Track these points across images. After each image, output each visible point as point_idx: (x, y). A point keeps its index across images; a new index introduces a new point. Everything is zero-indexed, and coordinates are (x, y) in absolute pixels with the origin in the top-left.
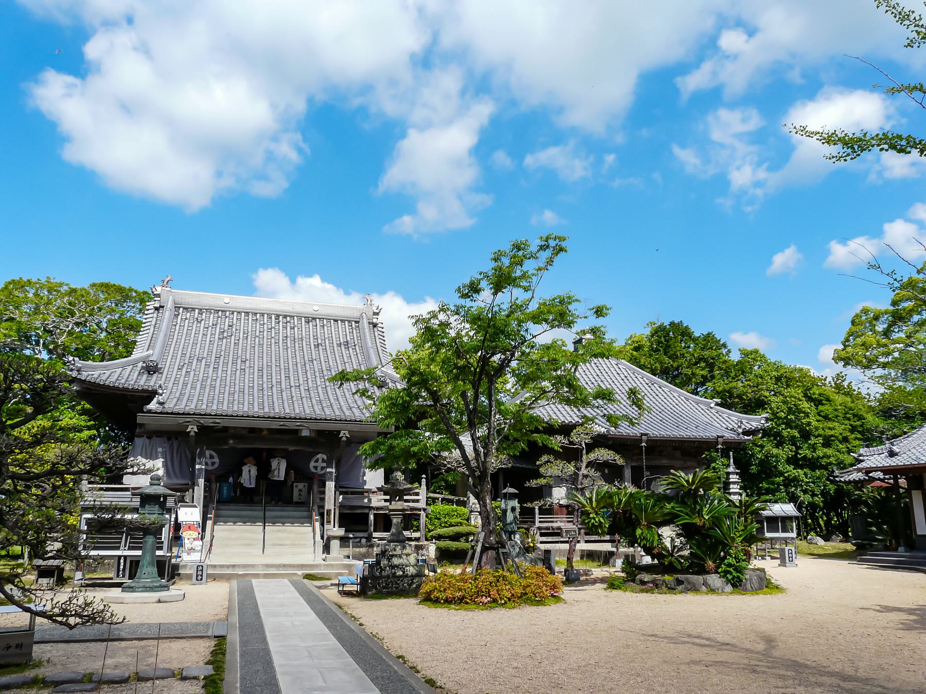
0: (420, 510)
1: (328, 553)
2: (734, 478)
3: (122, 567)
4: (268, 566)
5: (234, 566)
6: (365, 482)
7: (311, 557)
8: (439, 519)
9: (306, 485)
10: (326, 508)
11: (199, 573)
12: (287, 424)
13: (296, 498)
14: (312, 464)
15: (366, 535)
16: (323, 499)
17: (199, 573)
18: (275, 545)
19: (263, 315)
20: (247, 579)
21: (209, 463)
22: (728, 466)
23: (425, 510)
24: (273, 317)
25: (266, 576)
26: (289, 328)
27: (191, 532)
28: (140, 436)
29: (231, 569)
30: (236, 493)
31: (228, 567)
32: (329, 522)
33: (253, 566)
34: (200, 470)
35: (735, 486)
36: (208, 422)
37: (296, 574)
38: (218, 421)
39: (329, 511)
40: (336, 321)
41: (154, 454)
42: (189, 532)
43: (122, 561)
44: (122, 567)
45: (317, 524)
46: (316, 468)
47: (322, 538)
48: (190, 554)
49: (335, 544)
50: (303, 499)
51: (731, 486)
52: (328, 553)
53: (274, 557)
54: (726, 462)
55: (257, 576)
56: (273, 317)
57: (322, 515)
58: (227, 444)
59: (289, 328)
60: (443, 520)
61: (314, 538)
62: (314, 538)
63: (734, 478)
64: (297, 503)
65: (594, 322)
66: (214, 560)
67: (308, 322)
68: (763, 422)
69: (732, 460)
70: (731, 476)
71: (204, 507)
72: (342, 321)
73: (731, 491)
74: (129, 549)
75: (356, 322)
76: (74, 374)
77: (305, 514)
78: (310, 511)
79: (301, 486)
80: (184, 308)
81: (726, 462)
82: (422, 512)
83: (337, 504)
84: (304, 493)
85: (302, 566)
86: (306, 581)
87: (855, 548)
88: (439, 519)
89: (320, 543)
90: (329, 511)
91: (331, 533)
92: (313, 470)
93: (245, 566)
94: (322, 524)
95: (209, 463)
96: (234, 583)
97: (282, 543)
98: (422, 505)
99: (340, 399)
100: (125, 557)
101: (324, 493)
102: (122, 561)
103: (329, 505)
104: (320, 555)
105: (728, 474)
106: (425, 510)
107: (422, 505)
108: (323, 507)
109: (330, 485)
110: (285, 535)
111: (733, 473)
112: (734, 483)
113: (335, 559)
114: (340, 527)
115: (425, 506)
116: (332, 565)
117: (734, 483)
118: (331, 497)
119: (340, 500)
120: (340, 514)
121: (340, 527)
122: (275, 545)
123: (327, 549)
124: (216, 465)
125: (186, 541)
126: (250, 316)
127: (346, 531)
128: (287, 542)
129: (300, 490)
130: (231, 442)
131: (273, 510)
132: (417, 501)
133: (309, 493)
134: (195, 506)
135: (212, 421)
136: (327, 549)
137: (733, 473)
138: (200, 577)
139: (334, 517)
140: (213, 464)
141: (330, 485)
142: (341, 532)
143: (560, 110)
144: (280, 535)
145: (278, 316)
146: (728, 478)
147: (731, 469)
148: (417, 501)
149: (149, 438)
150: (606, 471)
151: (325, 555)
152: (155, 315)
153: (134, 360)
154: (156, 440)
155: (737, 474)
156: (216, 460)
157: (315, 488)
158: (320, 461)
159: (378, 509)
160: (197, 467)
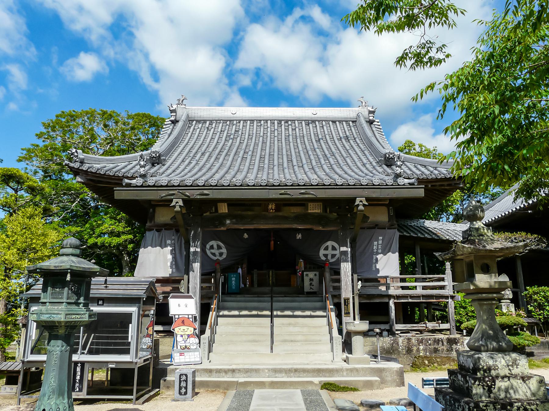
0: (447, 297)
1: (350, 352)
3: (78, 377)
4: (276, 371)
5: (233, 371)
6: (378, 271)
7: (329, 356)
8: (465, 308)
9: (317, 273)
10: (344, 295)
11: (183, 384)
12: (289, 191)
13: (307, 288)
14: (322, 252)
15: (387, 327)
16: (339, 288)
17: (183, 384)
18: (285, 341)
19: (266, 121)
20: (249, 389)
21: (217, 254)
23: (452, 297)
24: (276, 122)
25: (273, 385)
26: (290, 130)
27: (185, 328)
28: (150, 230)
29: (230, 374)
30: (245, 285)
31: (226, 371)
32: (348, 313)
33: (257, 371)
34: (195, 253)
36: (195, 194)
37: (311, 383)
38: (206, 192)
39: (347, 301)
40: (334, 122)
41: (163, 243)
42: (182, 328)
43: (78, 369)
44: (78, 377)
45: (333, 315)
46: (326, 256)
47: (340, 331)
48: (184, 354)
49: (357, 341)
50: (315, 288)
52: (350, 352)
53: (284, 357)
55: (261, 385)
56: (276, 122)
57: (338, 306)
58: (224, 225)
59: (290, 130)
60: (470, 308)
61: (330, 333)
62: (330, 333)
64: (308, 293)
66: (218, 361)
67: (308, 125)
71: (202, 297)
72: (340, 122)
74: (91, 352)
75: (353, 122)
76: (76, 165)
77: (319, 304)
78: (323, 301)
79: (311, 275)
80: (197, 121)
82: (450, 300)
83: (356, 292)
84: (316, 282)
85: (319, 372)
86: (324, 394)
88: (465, 308)
89: (338, 340)
90: (347, 301)
91: (352, 328)
92: (323, 258)
93: (247, 371)
94: (339, 316)
95: (217, 254)
96: (232, 393)
97: (292, 338)
98: (448, 291)
100: (83, 364)
101: (339, 281)
102: (78, 369)
103: (347, 292)
104: (341, 355)
106: (452, 297)
107: (448, 291)
108: (339, 296)
109: (346, 268)
110: (296, 329)
113: (360, 361)
114: (362, 319)
115: (452, 293)
116: (357, 370)
118: (348, 285)
119: (359, 287)
120: (360, 304)
121: (362, 319)
122: (285, 341)
123: (347, 346)
124: (224, 256)
125: (179, 339)
126: (255, 122)
127: (370, 323)
128: (299, 338)
129: (311, 280)
130: (228, 222)
131: (283, 301)
132: (442, 288)
133: (321, 282)
134: (190, 297)
135: (199, 192)
136: (347, 346)
138: (183, 390)
139: (353, 307)
140: (221, 254)
141: (346, 268)
142: (364, 326)
144: (291, 329)
145: (280, 122)
148: (442, 288)
149: (158, 231)
151: (345, 355)
152: (171, 127)
154: (164, 232)
156: (224, 250)
157: (327, 275)
158: (330, 248)
159: (398, 297)
160: (192, 249)
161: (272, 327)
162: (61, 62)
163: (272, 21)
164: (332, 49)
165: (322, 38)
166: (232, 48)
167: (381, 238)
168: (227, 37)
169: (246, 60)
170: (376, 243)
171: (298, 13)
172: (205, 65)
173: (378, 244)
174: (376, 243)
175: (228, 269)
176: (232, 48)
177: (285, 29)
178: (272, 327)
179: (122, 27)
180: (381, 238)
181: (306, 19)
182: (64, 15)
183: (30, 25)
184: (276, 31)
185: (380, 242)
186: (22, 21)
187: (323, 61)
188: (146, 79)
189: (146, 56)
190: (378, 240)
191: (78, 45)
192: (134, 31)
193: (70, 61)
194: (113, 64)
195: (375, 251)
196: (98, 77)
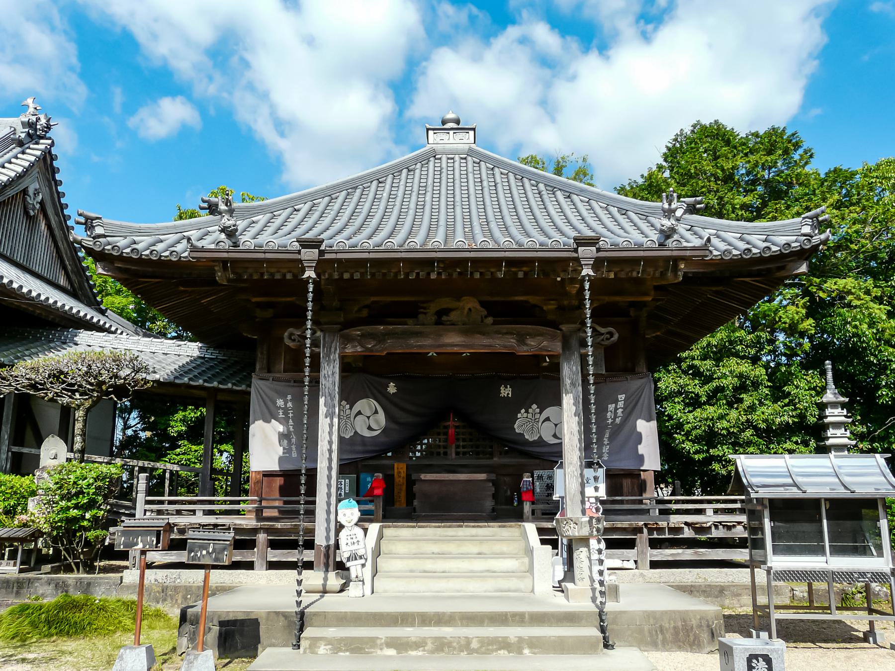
2: (835, 415)
22: (824, 389)
35: (840, 432)
51: (830, 432)
54: (817, 382)
63: (835, 415)
65: (597, 474)
68: (806, 230)
69: (830, 375)
70: (828, 412)
73: (831, 442)
81: (817, 382)
87: (560, 326)
99: (493, 225)
105: (822, 407)
111: (834, 405)
112: (837, 425)
117: (837, 425)
137: (834, 405)
143: (561, 466)
146: (822, 417)
147: (830, 396)
150: (392, 389)
153: (199, 223)
155: (843, 406)
161: (554, 571)
162: (130, 109)
163: (470, 44)
164: (563, 92)
165: (547, 72)
166: (403, 85)
167: (622, 397)
168: (397, 66)
169: (425, 107)
170: (611, 407)
171: (513, 32)
172: (358, 111)
173: (616, 409)
174: (611, 407)
175: (397, 443)
176: (403, 85)
177: (490, 56)
178: (554, 571)
179: (228, 51)
180: (622, 397)
181: (524, 41)
182: (142, 37)
183: (85, 54)
184: (477, 59)
185: (621, 404)
186: (72, 49)
187: (547, 107)
188: (264, 130)
189: (265, 96)
190: (616, 401)
191: (161, 82)
192: (248, 56)
193: (143, 113)
194: (212, 112)
195: (610, 421)
196: (184, 132)
